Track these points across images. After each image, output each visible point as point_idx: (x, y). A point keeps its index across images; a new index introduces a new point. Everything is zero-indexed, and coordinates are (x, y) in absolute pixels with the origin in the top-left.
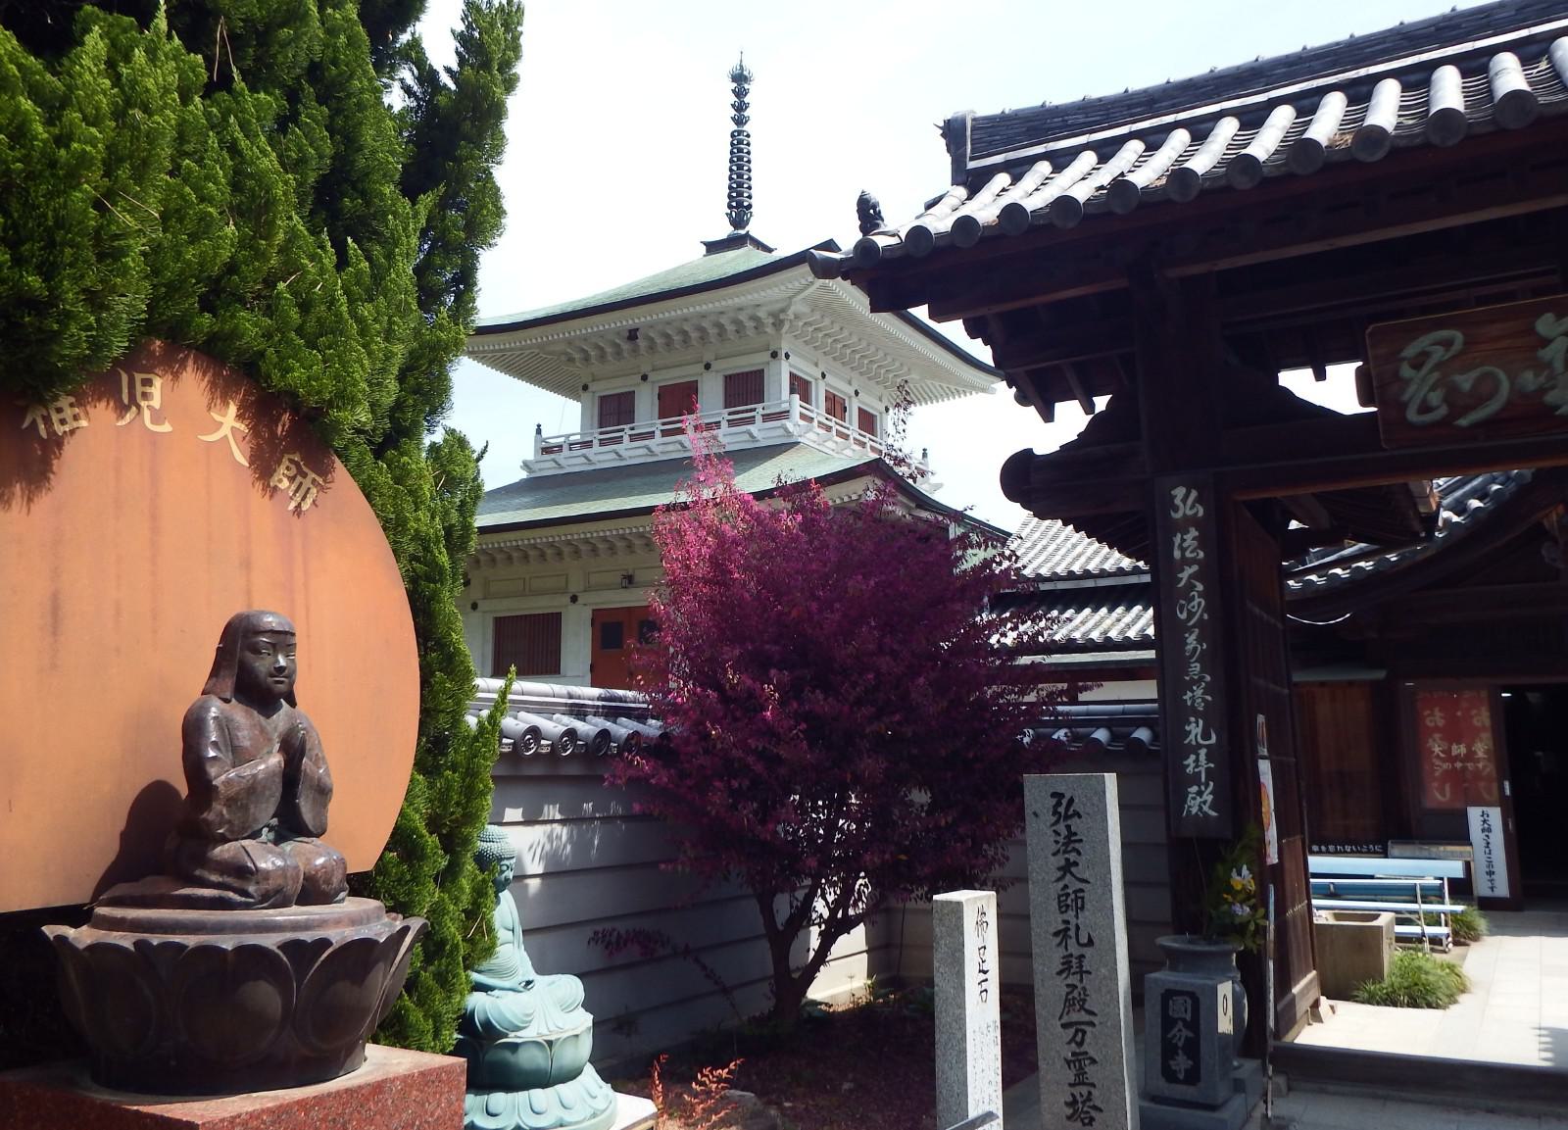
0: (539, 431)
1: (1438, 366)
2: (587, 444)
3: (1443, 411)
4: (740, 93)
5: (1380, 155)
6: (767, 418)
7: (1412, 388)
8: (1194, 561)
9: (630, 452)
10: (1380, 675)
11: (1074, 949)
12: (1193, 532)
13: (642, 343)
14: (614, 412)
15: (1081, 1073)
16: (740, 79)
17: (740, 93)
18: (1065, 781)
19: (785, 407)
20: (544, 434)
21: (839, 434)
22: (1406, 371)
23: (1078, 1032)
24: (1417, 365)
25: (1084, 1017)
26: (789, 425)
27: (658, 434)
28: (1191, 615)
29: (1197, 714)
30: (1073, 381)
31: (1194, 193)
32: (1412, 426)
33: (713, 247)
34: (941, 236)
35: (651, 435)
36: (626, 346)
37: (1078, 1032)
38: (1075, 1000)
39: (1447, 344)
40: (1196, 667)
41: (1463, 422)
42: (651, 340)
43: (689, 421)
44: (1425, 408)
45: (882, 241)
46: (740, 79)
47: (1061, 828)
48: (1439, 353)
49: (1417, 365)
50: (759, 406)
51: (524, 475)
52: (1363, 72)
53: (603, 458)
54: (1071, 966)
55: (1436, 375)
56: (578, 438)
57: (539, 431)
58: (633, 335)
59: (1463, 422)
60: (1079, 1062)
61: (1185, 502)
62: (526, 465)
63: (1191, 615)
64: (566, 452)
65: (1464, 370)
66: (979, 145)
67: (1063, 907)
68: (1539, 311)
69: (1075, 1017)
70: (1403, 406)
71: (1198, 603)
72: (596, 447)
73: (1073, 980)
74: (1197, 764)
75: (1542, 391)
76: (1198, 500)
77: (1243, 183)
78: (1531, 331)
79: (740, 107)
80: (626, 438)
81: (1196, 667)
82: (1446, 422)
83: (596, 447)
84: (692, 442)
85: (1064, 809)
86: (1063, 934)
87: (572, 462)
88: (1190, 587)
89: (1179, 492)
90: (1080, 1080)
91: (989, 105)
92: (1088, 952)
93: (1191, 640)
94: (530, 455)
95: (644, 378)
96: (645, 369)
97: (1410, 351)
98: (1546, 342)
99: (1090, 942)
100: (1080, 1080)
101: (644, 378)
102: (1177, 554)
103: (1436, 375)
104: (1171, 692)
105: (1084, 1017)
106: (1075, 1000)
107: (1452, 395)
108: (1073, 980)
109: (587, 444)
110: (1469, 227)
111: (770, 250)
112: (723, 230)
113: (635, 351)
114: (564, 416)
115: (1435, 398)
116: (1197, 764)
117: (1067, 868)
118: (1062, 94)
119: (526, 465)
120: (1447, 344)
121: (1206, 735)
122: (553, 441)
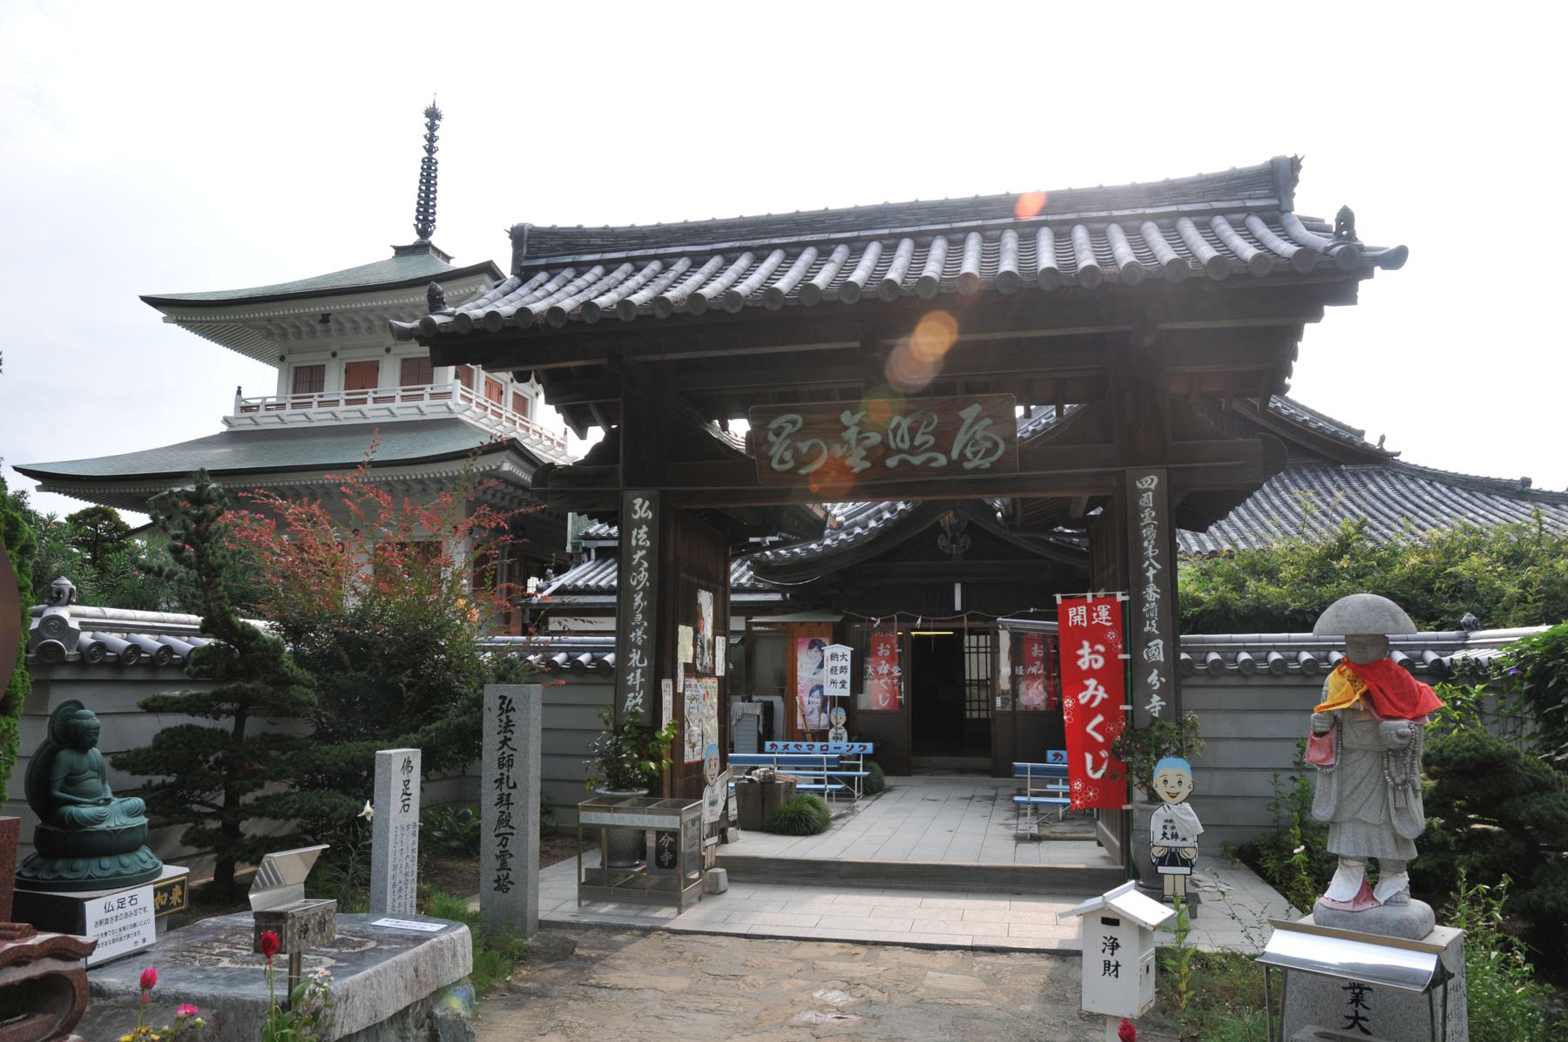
0: (239, 392)
1: (789, 436)
2: (281, 406)
3: (791, 465)
4: (432, 128)
5: (737, 310)
6: (433, 396)
7: (774, 449)
8: (642, 548)
9: (318, 416)
10: (838, 619)
11: (505, 790)
12: (645, 529)
13: (332, 325)
14: (305, 380)
15: (504, 863)
16: (433, 115)
17: (432, 128)
18: (506, 689)
19: (449, 389)
20: (244, 395)
21: (494, 412)
22: (771, 437)
23: (504, 838)
24: (778, 434)
25: (507, 830)
26: (450, 403)
27: (342, 402)
28: (639, 583)
29: (637, 647)
30: (597, 416)
31: (633, 317)
32: (773, 470)
33: (401, 251)
34: (478, 320)
35: (336, 403)
36: (319, 327)
37: (504, 838)
38: (504, 820)
39: (794, 423)
40: (639, 617)
41: (803, 472)
42: (340, 324)
43: (370, 394)
44: (782, 461)
45: (438, 319)
46: (433, 115)
47: (504, 717)
48: (789, 429)
49: (778, 434)
50: (428, 387)
51: (224, 428)
52: (766, 241)
53: (294, 418)
54: (504, 800)
55: (788, 442)
56: (274, 400)
57: (239, 392)
58: (325, 318)
59: (803, 472)
60: (503, 856)
61: (641, 508)
62: (226, 420)
63: (639, 583)
64: (262, 412)
65: (803, 440)
66: (540, 250)
67: (501, 766)
68: (842, 409)
69: (503, 830)
70: (770, 459)
71: (644, 576)
72: (288, 409)
73: (504, 808)
74: (635, 679)
75: (844, 457)
76: (649, 508)
77: (661, 314)
78: (838, 421)
79: (431, 139)
80: (315, 404)
81: (639, 617)
82: (793, 471)
83: (288, 409)
84: (373, 412)
85: (506, 706)
86: (499, 781)
87: (268, 422)
88: (640, 564)
89: (638, 501)
90: (504, 866)
91: (542, 221)
92: (513, 792)
93: (638, 598)
94: (230, 412)
95: (334, 355)
96: (335, 348)
97: (774, 425)
98: (846, 428)
99: (515, 786)
100: (504, 866)
101: (334, 355)
102: (634, 542)
103: (788, 442)
104: (622, 632)
105: (507, 830)
106: (504, 820)
107: (796, 454)
108: (504, 808)
109: (281, 406)
110: (797, 353)
111: (447, 258)
112: (411, 238)
113: (327, 332)
114: (261, 379)
115: (788, 456)
116: (635, 679)
117: (505, 742)
118: (592, 219)
119: (226, 420)
120: (794, 423)
121: (641, 661)
122: (253, 402)
